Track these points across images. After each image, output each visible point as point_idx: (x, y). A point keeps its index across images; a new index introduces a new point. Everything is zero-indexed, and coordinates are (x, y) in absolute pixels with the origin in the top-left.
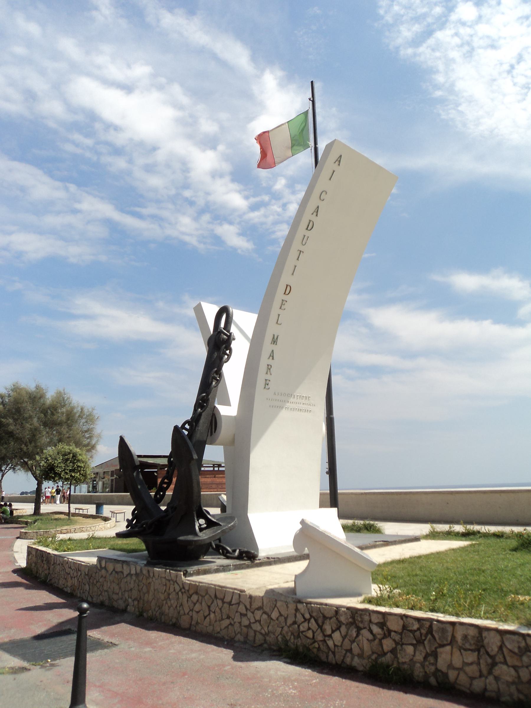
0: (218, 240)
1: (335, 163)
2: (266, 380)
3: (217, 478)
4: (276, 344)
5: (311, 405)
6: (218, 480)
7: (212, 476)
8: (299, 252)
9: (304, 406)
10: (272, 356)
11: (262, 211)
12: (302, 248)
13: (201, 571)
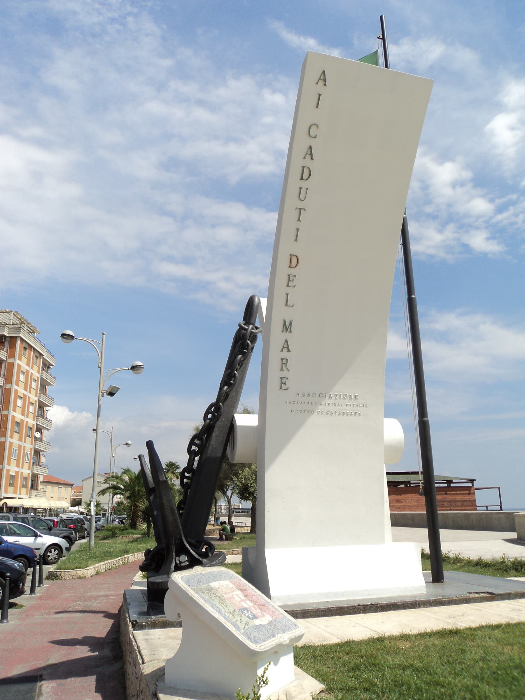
0: (466, 248)
1: (317, 83)
2: (281, 378)
3: (448, 496)
4: (291, 332)
5: (360, 406)
6: (449, 497)
7: (442, 493)
8: (298, 211)
9: (348, 408)
10: (286, 346)
11: (511, 210)
12: (301, 205)
13: (158, 623)
